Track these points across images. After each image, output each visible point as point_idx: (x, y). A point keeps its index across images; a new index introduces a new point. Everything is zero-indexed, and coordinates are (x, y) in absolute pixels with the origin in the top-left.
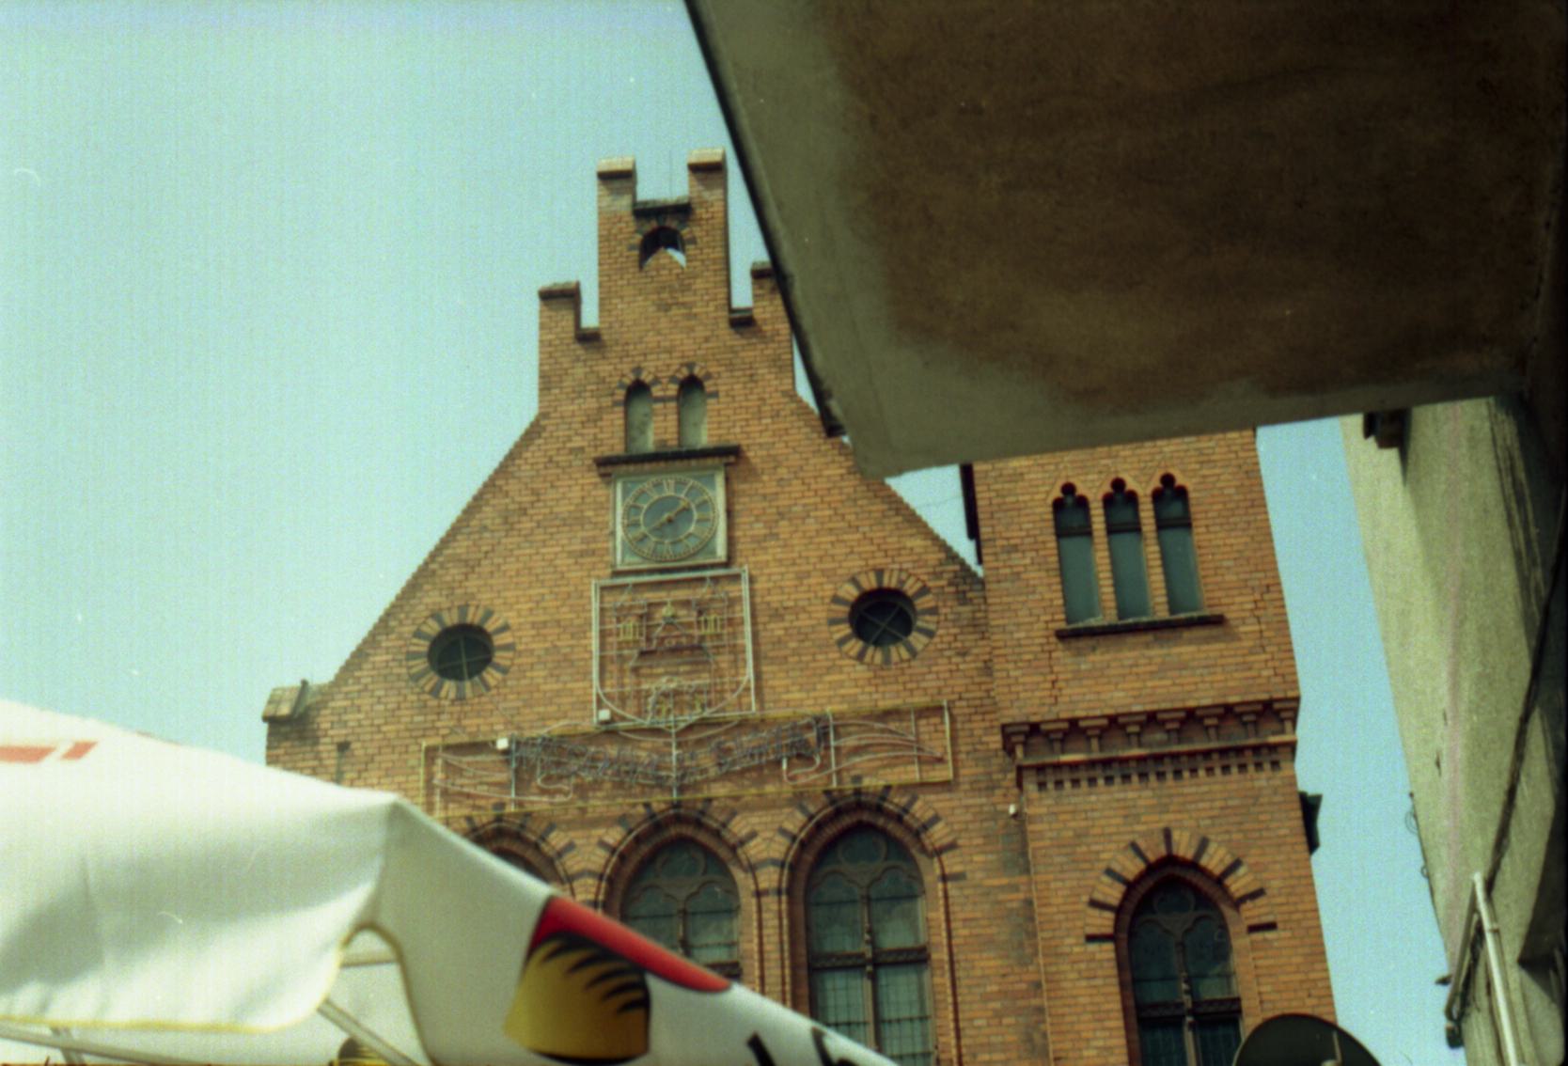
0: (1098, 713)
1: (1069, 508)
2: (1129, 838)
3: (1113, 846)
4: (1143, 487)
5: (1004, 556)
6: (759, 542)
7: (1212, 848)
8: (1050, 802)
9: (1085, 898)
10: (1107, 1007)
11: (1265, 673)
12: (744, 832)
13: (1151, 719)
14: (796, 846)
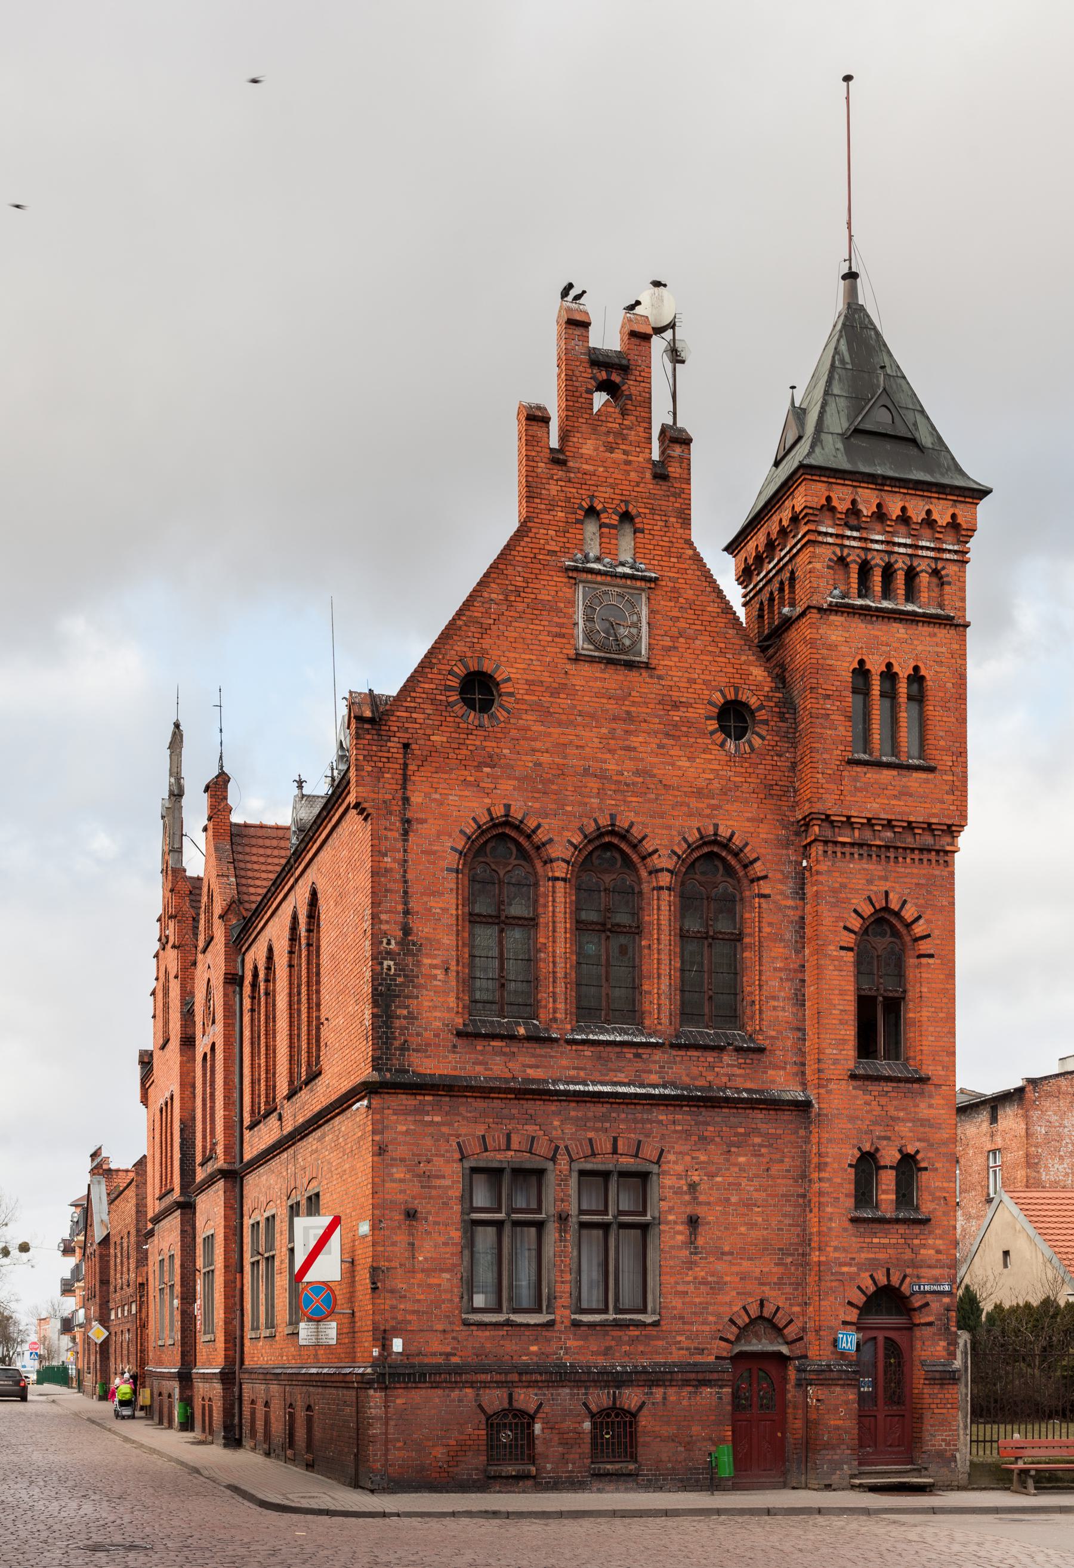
2: (868, 893)
6: (668, 649)
7: (908, 906)
8: (829, 863)
9: (842, 924)
10: (847, 988)
11: (952, 808)
12: (650, 850)
13: (889, 824)
14: (624, 832)
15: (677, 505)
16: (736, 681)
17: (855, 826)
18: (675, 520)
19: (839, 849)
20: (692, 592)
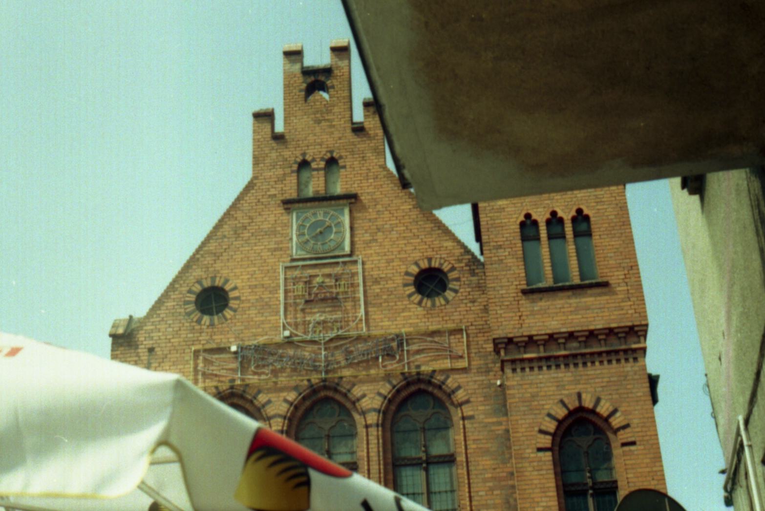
0: (543, 332)
1: (528, 226)
2: (559, 397)
3: (551, 402)
4: (567, 215)
5: (494, 251)
7: (602, 403)
8: (518, 378)
9: (536, 429)
10: (547, 485)
11: (630, 312)
12: (359, 394)
13: (571, 336)
15: (371, 145)
16: (429, 254)
17: (539, 343)
18: (371, 155)
19: (527, 365)
20: (387, 199)
